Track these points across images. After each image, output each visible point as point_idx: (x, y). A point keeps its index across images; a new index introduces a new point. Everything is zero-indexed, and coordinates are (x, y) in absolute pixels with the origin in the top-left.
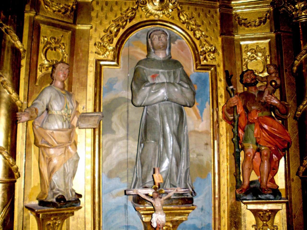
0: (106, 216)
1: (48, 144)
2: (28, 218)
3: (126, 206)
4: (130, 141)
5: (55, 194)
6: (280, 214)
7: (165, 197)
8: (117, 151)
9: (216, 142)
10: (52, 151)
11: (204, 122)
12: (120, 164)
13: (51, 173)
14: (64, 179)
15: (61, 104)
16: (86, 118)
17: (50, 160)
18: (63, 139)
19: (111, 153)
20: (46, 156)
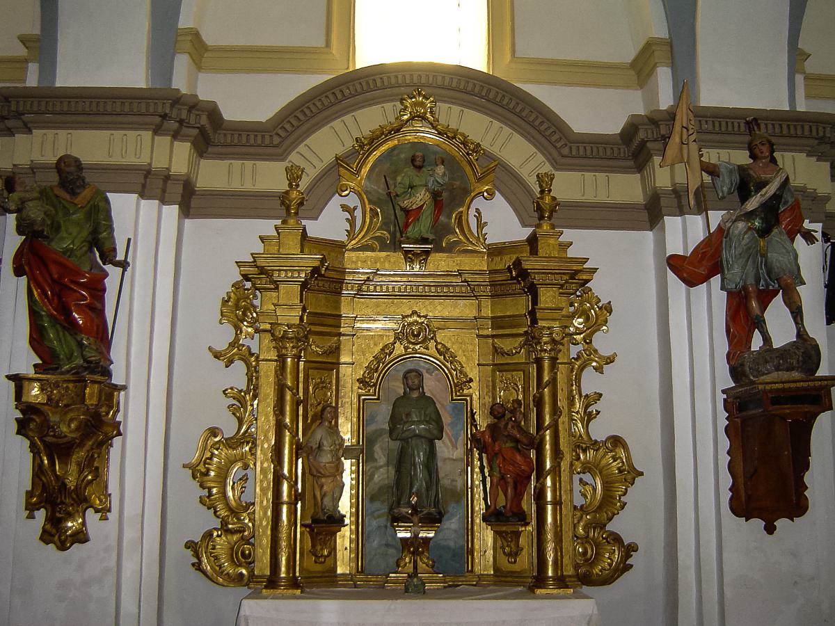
0: (369, 534)
1: (321, 473)
2: (78, 163)
3: (386, 527)
4: (390, 468)
5: (325, 513)
6: (41, 181)
7: (420, 515)
8: (379, 477)
9: (469, 468)
10: (323, 480)
11: (459, 450)
12: (381, 488)
13: (323, 497)
14: (54, 152)
15: (330, 441)
16: (351, 451)
17: (322, 487)
18: (332, 471)
19: (373, 478)
20: (319, 483)
